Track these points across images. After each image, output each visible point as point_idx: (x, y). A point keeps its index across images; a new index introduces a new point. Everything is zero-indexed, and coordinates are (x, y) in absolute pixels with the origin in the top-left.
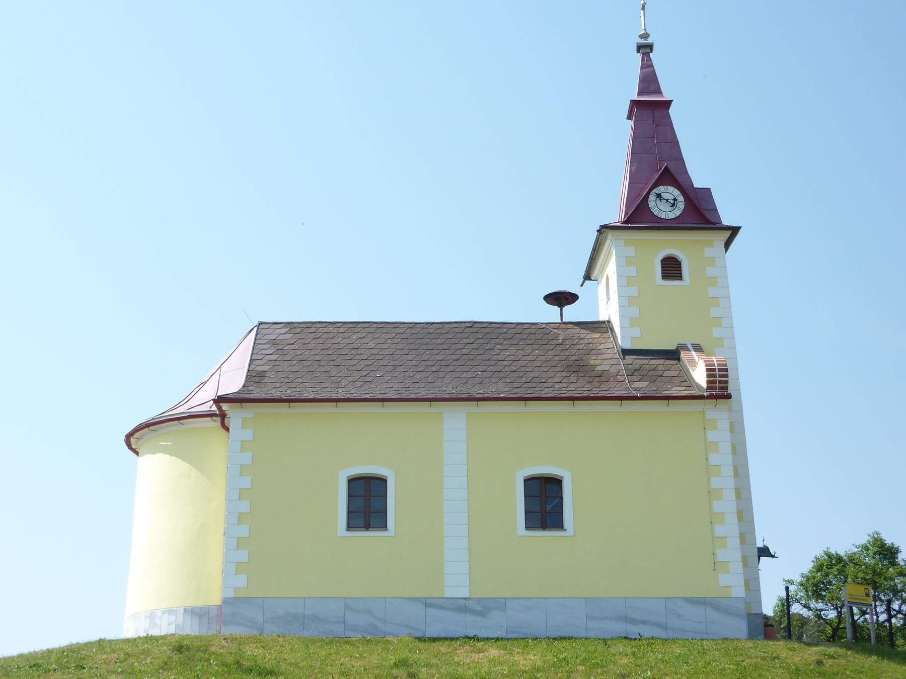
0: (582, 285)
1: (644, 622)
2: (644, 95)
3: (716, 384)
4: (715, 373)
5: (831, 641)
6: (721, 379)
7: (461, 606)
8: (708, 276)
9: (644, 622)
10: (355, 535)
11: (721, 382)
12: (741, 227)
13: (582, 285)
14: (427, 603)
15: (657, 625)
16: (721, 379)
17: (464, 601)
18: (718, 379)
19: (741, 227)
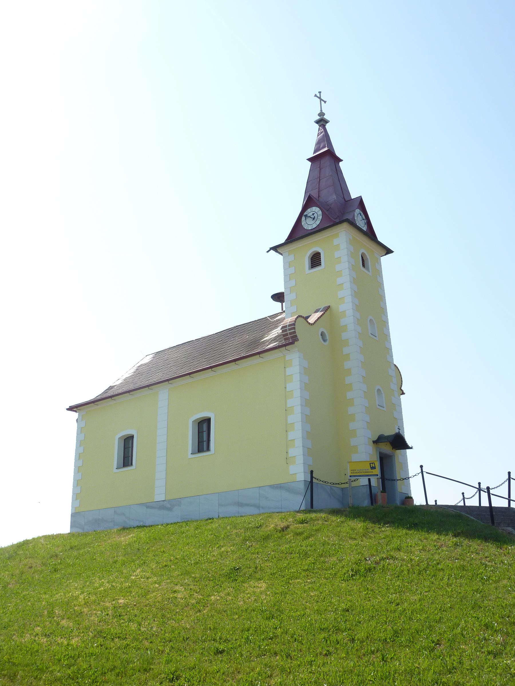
0: (268, 252)
1: (247, 505)
2: (399, 475)
3: (288, 335)
4: (288, 336)
5: (412, 526)
6: (289, 327)
7: (162, 506)
8: (339, 298)
9: (247, 505)
10: (129, 469)
11: (291, 333)
12: (307, 159)
13: (268, 252)
14: (148, 506)
15: (254, 506)
16: (289, 327)
17: (162, 502)
18: (288, 332)
19: (307, 159)
